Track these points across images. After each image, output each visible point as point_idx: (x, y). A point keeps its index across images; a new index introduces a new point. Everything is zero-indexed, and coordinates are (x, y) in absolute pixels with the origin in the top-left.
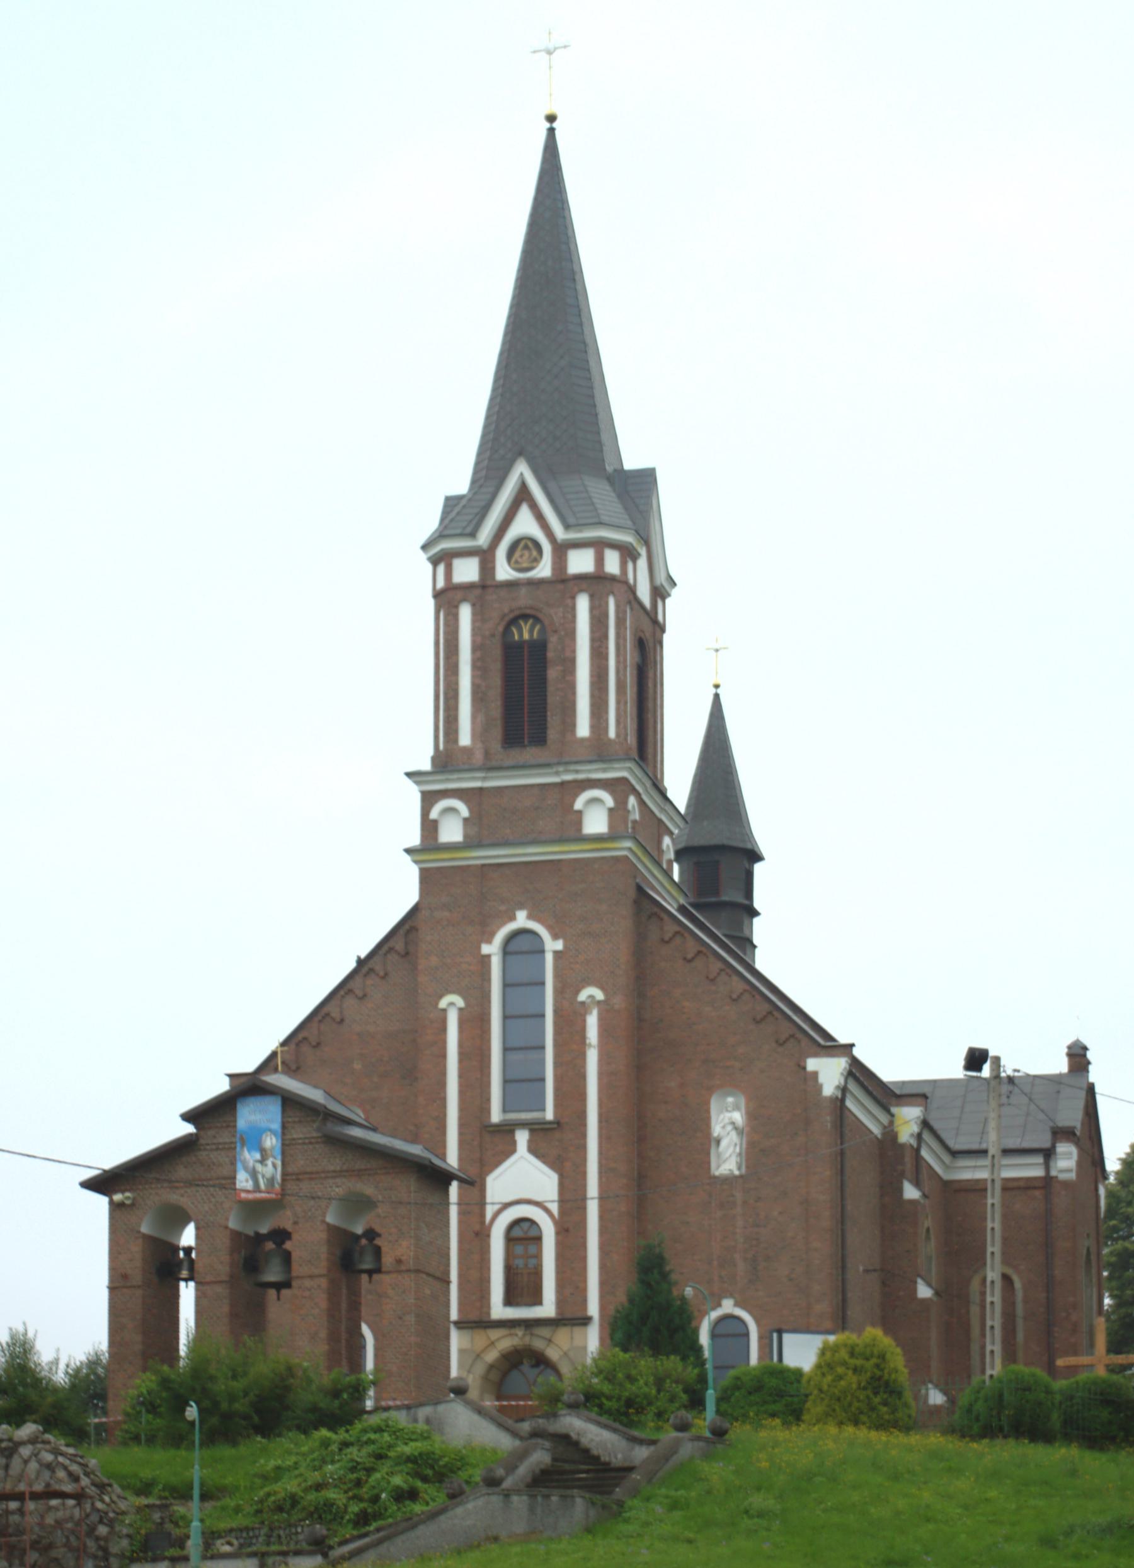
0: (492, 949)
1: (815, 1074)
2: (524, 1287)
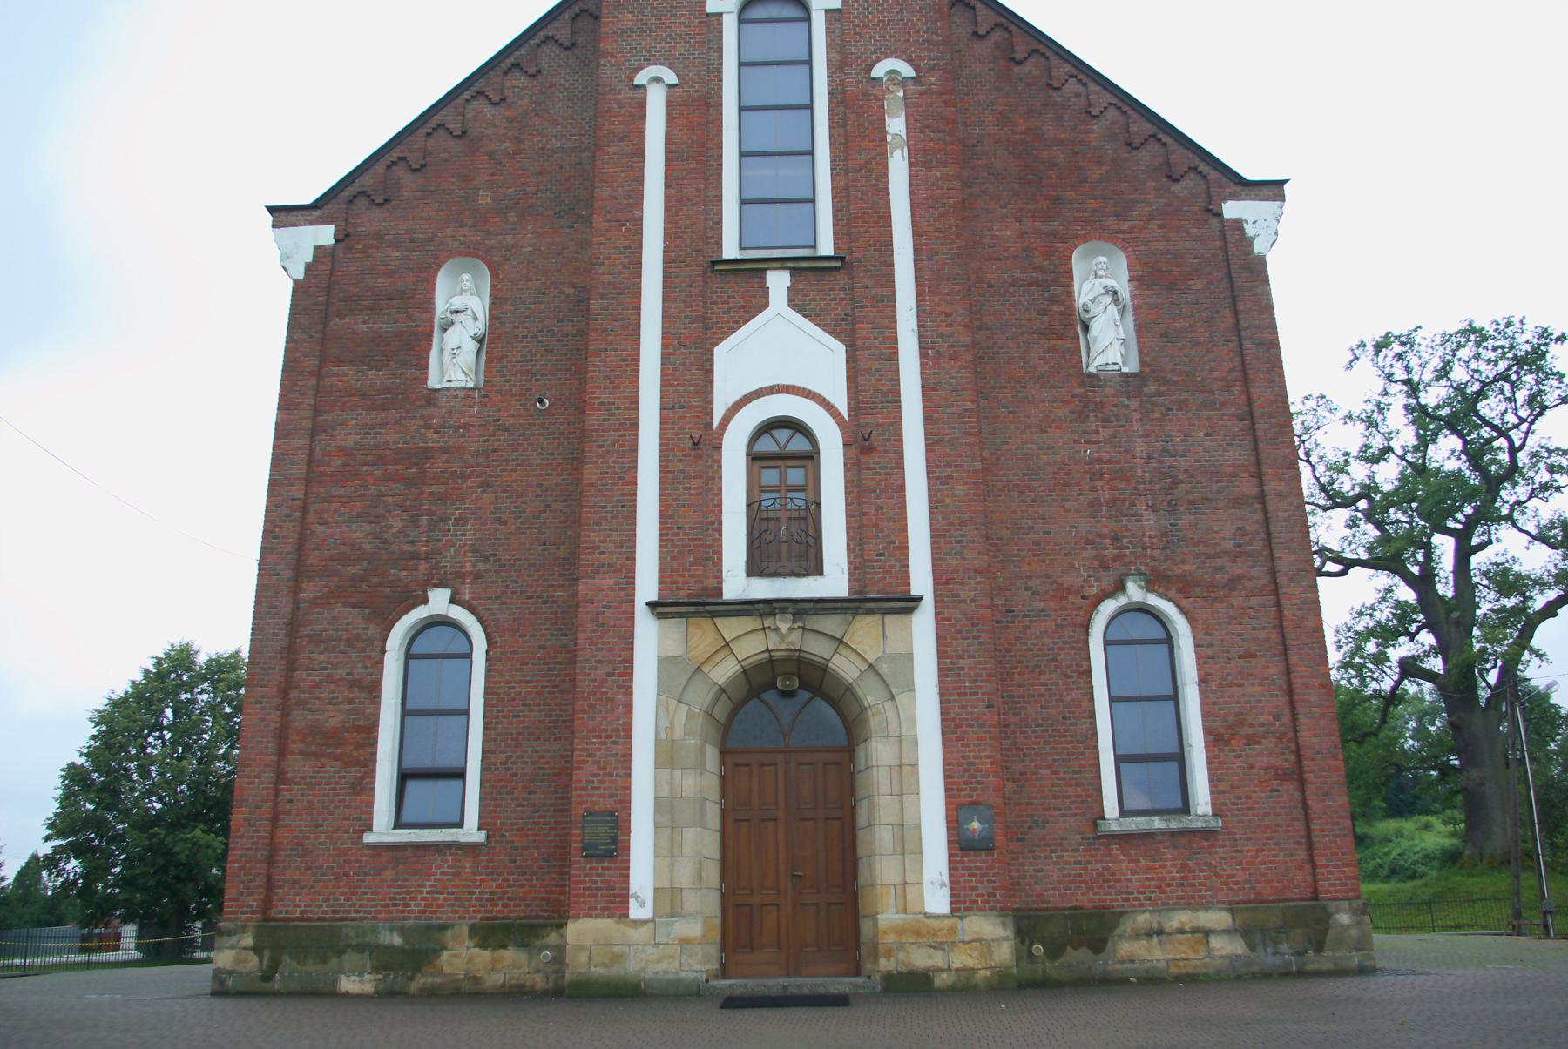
1: (1238, 224)
2: (784, 541)
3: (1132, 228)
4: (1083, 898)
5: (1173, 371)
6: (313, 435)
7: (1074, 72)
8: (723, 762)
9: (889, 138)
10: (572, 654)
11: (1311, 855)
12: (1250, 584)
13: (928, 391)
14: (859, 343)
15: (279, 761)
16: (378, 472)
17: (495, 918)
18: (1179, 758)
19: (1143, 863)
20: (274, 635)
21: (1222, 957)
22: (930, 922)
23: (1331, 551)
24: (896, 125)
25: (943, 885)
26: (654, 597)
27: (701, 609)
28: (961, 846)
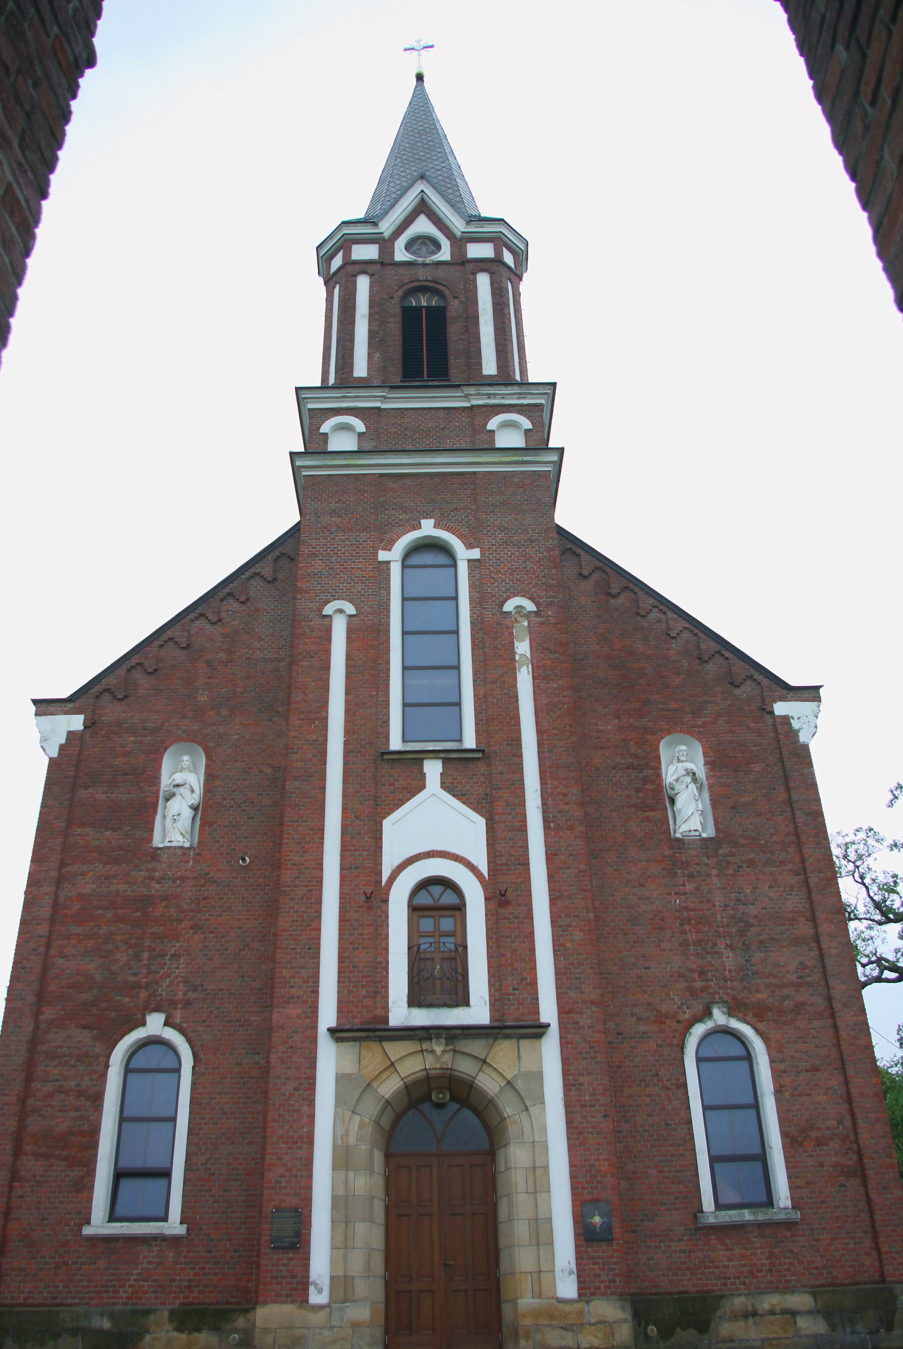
0: (393, 555)
1: (786, 720)
2: (436, 978)
3: (705, 723)
4: (688, 1284)
5: (741, 836)
6: (58, 883)
7: (656, 603)
8: (387, 1164)
9: (517, 658)
10: (265, 1072)
11: (876, 1243)
12: (811, 1009)
13: (551, 857)
14: (496, 817)
15: (14, 1162)
16: (110, 915)
17: (192, 1304)
18: (762, 1158)
19: (737, 1251)
20: (17, 1051)
21: (807, 1336)
22: (560, 1306)
23: (887, 961)
24: (523, 648)
25: (571, 1273)
26: (333, 1024)
27: (371, 1034)
28: (586, 1236)
